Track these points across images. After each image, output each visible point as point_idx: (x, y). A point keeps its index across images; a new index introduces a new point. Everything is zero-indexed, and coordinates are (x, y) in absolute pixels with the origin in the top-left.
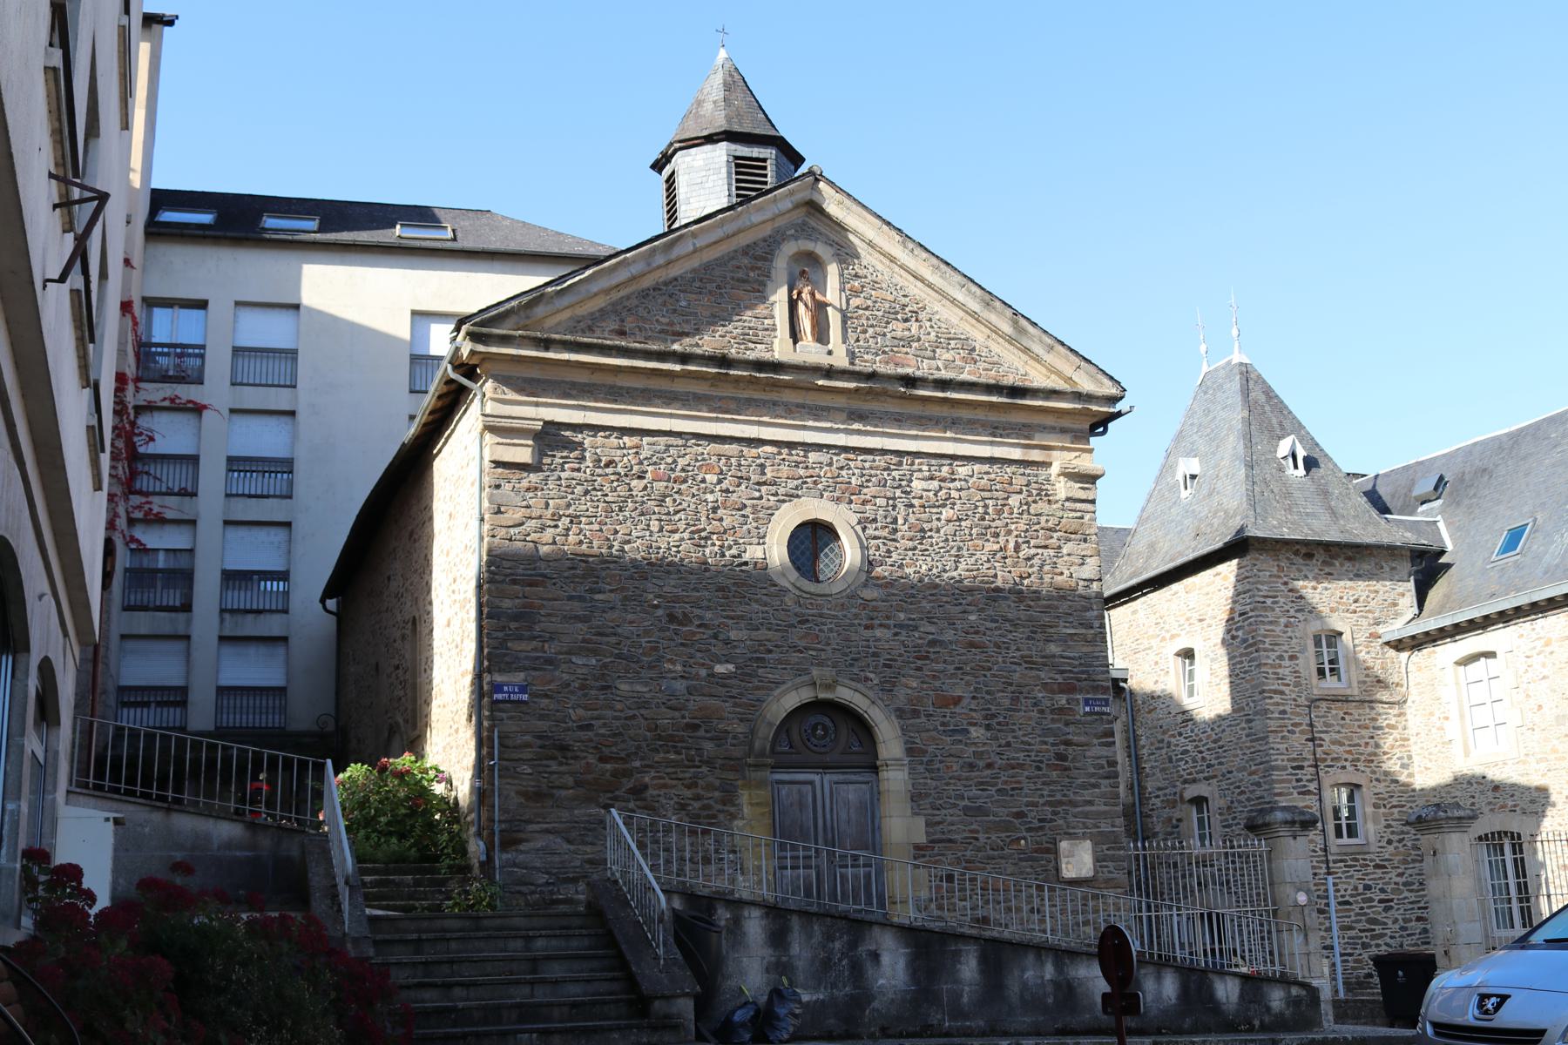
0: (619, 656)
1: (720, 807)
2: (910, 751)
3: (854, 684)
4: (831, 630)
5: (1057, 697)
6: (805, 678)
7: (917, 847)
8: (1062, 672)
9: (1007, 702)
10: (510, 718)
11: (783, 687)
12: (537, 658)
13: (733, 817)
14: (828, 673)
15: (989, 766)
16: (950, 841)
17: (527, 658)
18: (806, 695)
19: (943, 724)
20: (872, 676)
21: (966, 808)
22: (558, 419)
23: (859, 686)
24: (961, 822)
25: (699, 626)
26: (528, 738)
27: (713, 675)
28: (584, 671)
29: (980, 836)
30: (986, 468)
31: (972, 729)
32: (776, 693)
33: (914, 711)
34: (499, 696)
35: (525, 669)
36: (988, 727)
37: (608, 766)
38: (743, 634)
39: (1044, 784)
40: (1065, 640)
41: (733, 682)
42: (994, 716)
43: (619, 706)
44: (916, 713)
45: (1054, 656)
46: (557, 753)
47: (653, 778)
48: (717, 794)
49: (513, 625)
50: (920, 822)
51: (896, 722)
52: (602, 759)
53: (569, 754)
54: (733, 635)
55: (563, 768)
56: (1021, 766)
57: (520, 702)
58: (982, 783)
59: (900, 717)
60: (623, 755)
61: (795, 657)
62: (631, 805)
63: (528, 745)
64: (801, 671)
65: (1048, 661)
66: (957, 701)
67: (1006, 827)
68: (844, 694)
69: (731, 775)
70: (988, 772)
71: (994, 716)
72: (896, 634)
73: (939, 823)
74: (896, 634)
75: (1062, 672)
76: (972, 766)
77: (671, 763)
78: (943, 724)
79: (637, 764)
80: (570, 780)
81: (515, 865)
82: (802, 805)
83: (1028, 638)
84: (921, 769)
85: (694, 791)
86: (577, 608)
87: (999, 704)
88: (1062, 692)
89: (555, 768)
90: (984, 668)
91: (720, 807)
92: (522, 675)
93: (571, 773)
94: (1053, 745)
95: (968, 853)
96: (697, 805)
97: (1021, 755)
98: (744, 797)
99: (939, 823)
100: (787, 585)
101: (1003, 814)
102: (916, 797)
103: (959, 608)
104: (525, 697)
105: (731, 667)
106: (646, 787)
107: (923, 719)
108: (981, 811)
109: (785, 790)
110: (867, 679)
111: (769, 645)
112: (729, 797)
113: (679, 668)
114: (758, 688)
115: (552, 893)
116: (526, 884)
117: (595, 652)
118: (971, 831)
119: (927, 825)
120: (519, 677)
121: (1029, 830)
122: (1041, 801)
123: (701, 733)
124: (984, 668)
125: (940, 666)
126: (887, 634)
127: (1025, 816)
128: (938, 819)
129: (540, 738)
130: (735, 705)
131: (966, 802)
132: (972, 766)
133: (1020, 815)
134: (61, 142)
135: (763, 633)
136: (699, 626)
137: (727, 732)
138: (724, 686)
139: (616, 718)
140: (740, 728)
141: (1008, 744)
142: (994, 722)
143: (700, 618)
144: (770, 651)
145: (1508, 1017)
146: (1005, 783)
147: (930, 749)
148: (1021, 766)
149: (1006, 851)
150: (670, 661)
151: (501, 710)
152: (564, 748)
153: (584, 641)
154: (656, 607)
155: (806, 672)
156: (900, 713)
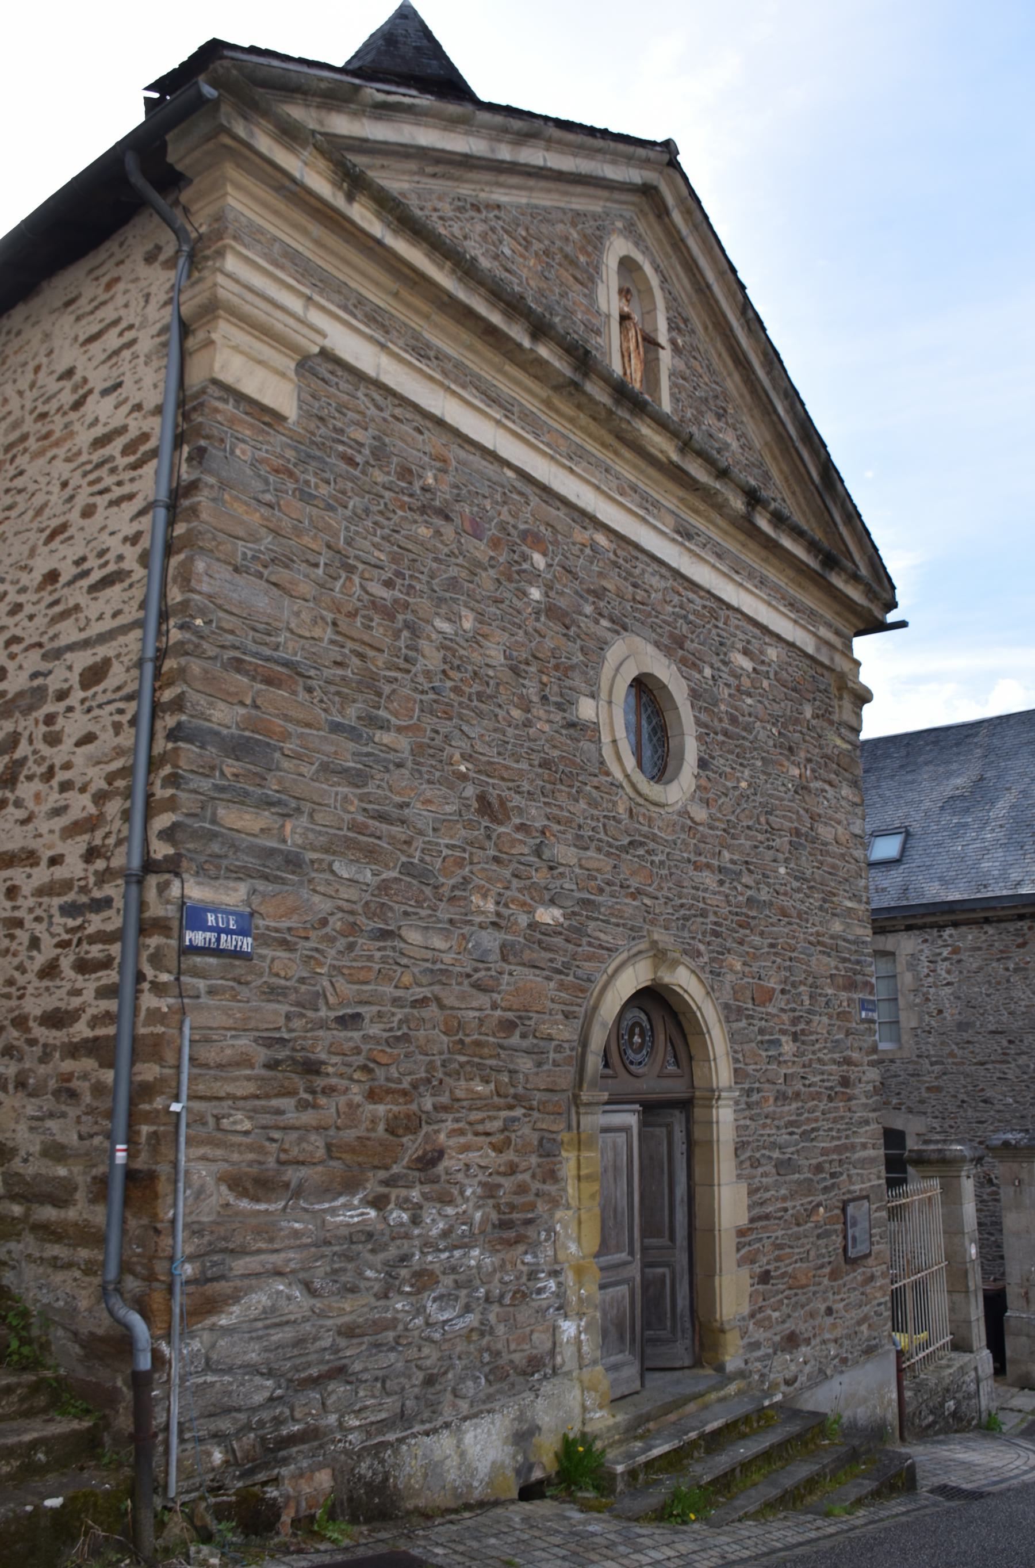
8: (845, 960)
10: (211, 992)
12: (271, 852)
13: (555, 1203)
17: (252, 850)
22: (465, 429)
26: (244, 1042)
28: (352, 893)
30: (757, 632)
34: (196, 937)
35: (240, 873)
37: (381, 1109)
41: (558, 941)
46: (299, 1082)
47: (452, 1133)
49: (231, 767)
52: (372, 1096)
53: (320, 1082)
55: (308, 1117)
57: (236, 954)
60: (405, 1085)
62: (415, 1195)
63: (244, 1061)
77: (477, 1102)
80: (317, 1143)
81: (209, 1367)
86: (346, 752)
89: (292, 1117)
92: (242, 890)
93: (320, 1128)
98: (568, 1163)
104: (246, 944)
113: (491, 906)
115: (278, 1422)
116: (228, 1410)
117: (371, 854)
120: (234, 895)
129: (269, 1043)
134: (615, 153)
139: (396, 1001)
151: (196, 973)
152: (311, 1068)
153: (354, 827)
154: (463, 777)
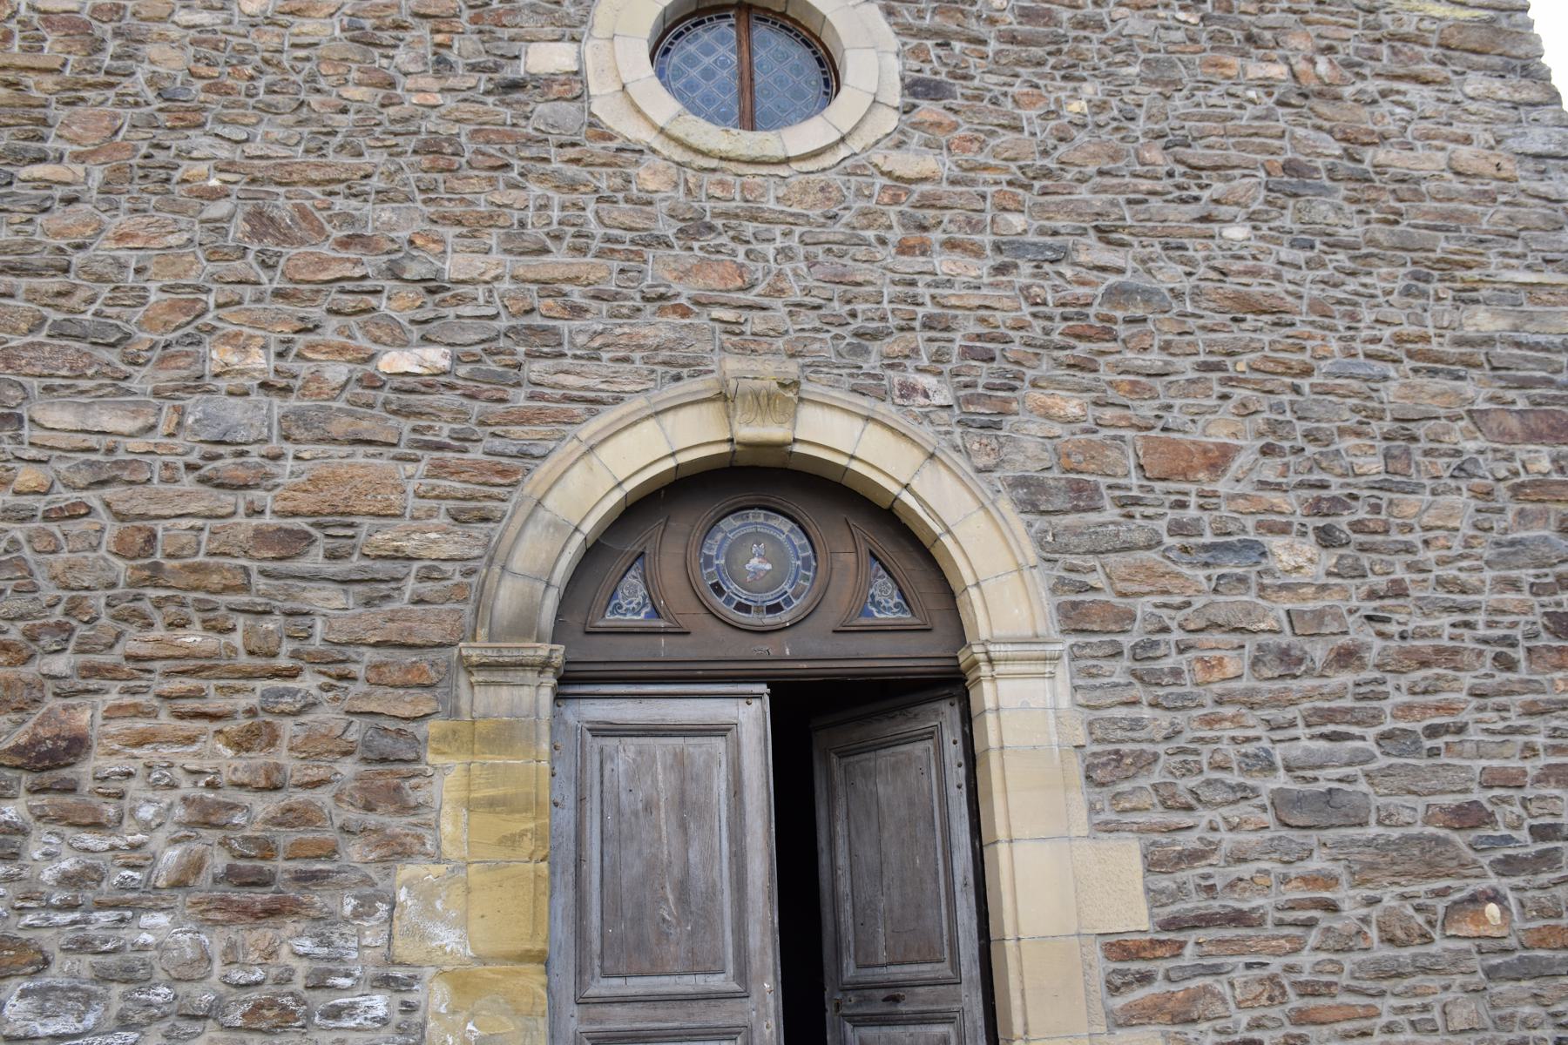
0: (59, 332)
1: (353, 815)
2: (1074, 618)
3: (865, 403)
4: (785, 253)
5: (1522, 451)
6: (692, 386)
7: (1120, 949)
8: (1524, 384)
9: (1373, 465)
11: (609, 416)
13: (397, 851)
14: (768, 370)
15: (1347, 657)
16: (1238, 918)
18: (695, 434)
19: (1177, 529)
20: (927, 381)
21: (1281, 801)
23: (883, 409)
24: (1270, 849)
25: (345, 243)
27: (373, 383)
29: (1347, 896)
31: (1275, 543)
32: (590, 429)
33: (1078, 489)
36: (1326, 538)
38: (494, 263)
39: (1530, 711)
40: (1511, 297)
42: (1340, 504)
43: (27, 476)
44: (1083, 496)
45: (1488, 341)
47: (112, 714)
48: (348, 768)
50: (1127, 855)
51: (1017, 521)
54: (454, 266)
56: (1449, 656)
58: (1329, 716)
59: (1030, 506)
61: (658, 328)
64: (679, 367)
65: (1472, 355)
66: (1219, 459)
67: (1428, 859)
68: (829, 432)
69: (406, 704)
70: (1346, 678)
71: (1340, 504)
72: (1001, 269)
73: (1194, 856)
74: (1001, 269)
75: (1524, 384)
76: (1289, 660)
77: (201, 666)
78: (1177, 529)
79: (60, 664)
82: (687, 808)
83: (1407, 292)
84: (1118, 670)
85: (259, 758)
87: (1350, 472)
88: (1534, 436)
90: (1288, 370)
91: (353, 815)
94: (1536, 590)
95: (1306, 959)
96: (264, 806)
97: (1445, 620)
98: (447, 779)
99: (1194, 856)
100: (646, 136)
101: (1413, 816)
102: (1107, 768)
103: (1193, 210)
105: (437, 357)
106: (77, 745)
107: (1111, 513)
108: (1331, 809)
109: (625, 752)
110: (908, 390)
111: (576, 295)
112: (390, 767)
114: (524, 419)
118: (1309, 880)
119: (1154, 864)
121: (1508, 866)
122: (1533, 766)
123: (314, 560)
124: (1288, 370)
125: (1155, 359)
126: (979, 269)
127: (1487, 819)
128: (1189, 841)
130: (438, 470)
131: (1282, 780)
132: (1289, 660)
133: (1468, 817)
135: (559, 261)
136: (345, 243)
137: (398, 556)
138: (403, 412)
140: (440, 541)
141: (1398, 590)
142: (1343, 521)
143: (348, 219)
144: (578, 311)
145: (962, 760)
146: (1406, 710)
147: (1143, 606)
148: (1449, 656)
149: (1439, 945)
150: (230, 340)
154: (215, 195)
155: (695, 367)
156: (1031, 495)
